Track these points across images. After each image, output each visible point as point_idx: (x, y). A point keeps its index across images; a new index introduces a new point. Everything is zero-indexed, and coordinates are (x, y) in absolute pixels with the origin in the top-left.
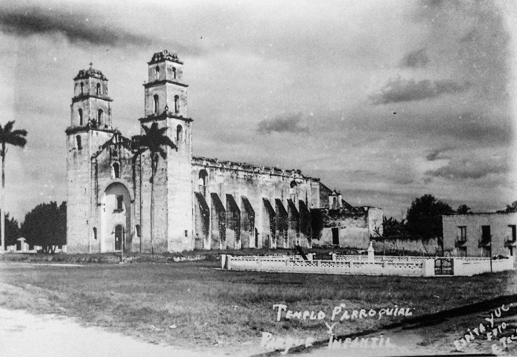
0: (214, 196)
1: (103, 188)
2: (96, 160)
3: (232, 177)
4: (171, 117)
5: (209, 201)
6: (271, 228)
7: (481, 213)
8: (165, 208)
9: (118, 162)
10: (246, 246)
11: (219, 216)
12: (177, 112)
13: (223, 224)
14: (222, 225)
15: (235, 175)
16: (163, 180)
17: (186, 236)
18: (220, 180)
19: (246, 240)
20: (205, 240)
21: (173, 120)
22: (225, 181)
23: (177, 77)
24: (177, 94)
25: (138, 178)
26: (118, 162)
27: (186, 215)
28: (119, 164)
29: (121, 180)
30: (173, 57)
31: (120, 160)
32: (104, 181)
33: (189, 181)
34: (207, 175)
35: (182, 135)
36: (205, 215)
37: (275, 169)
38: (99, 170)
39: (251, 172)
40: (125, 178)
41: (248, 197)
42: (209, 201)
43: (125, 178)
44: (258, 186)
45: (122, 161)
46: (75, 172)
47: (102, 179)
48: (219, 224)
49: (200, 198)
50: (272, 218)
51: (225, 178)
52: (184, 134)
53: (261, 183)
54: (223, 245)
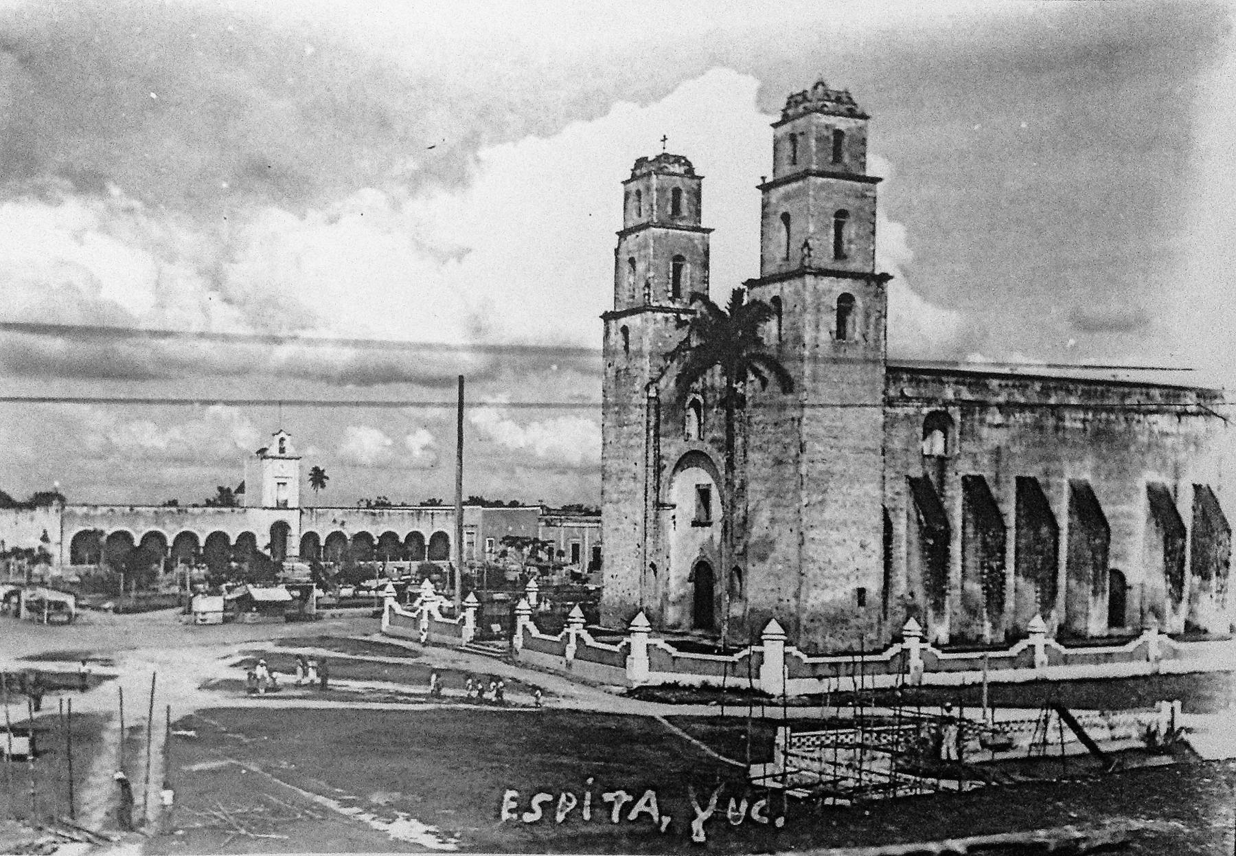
0: (975, 488)
1: (669, 465)
2: (658, 391)
3: (1041, 428)
4: (822, 273)
5: (955, 502)
6: (1167, 571)
7: (1124, 738)
8: (795, 527)
9: (699, 397)
10: (1078, 625)
11: (984, 542)
12: (839, 254)
13: (995, 564)
14: (990, 568)
15: (1051, 422)
16: (793, 451)
17: (861, 603)
18: (996, 438)
19: (1078, 607)
20: (931, 613)
21: (826, 282)
22: (1013, 439)
23: (846, 159)
24: (843, 207)
25: (739, 441)
26: (699, 397)
27: (863, 546)
28: (702, 402)
29: (708, 448)
30: (838, 100)
31: (703, 393)
32: (673, 449)
33: (874, 451)
34: (952, 422)
35: (854, 322)
36: (931, 542)
37: (1202, 394)
38: (662, 417)
39: (1110, 410)
40: (713, 441)
41: (1093, 484)
42: (955, 502)
43: (713, 441)
44: (1133, 448)
45: (709, 395)
46: (617, 421)
47: (668, 440)
48: (983, 567)
49: (926, 496)
50: (1173, 544)
51: (1014, 431)
52: (859, 319)
53: (1143, 439)
54: (995, 627)
